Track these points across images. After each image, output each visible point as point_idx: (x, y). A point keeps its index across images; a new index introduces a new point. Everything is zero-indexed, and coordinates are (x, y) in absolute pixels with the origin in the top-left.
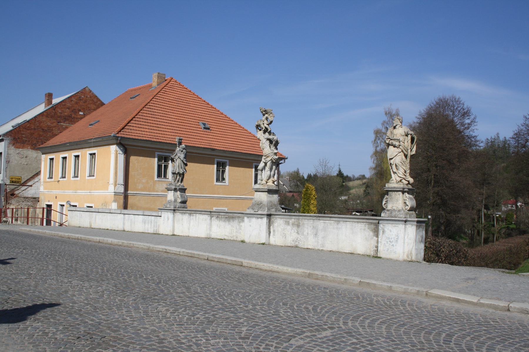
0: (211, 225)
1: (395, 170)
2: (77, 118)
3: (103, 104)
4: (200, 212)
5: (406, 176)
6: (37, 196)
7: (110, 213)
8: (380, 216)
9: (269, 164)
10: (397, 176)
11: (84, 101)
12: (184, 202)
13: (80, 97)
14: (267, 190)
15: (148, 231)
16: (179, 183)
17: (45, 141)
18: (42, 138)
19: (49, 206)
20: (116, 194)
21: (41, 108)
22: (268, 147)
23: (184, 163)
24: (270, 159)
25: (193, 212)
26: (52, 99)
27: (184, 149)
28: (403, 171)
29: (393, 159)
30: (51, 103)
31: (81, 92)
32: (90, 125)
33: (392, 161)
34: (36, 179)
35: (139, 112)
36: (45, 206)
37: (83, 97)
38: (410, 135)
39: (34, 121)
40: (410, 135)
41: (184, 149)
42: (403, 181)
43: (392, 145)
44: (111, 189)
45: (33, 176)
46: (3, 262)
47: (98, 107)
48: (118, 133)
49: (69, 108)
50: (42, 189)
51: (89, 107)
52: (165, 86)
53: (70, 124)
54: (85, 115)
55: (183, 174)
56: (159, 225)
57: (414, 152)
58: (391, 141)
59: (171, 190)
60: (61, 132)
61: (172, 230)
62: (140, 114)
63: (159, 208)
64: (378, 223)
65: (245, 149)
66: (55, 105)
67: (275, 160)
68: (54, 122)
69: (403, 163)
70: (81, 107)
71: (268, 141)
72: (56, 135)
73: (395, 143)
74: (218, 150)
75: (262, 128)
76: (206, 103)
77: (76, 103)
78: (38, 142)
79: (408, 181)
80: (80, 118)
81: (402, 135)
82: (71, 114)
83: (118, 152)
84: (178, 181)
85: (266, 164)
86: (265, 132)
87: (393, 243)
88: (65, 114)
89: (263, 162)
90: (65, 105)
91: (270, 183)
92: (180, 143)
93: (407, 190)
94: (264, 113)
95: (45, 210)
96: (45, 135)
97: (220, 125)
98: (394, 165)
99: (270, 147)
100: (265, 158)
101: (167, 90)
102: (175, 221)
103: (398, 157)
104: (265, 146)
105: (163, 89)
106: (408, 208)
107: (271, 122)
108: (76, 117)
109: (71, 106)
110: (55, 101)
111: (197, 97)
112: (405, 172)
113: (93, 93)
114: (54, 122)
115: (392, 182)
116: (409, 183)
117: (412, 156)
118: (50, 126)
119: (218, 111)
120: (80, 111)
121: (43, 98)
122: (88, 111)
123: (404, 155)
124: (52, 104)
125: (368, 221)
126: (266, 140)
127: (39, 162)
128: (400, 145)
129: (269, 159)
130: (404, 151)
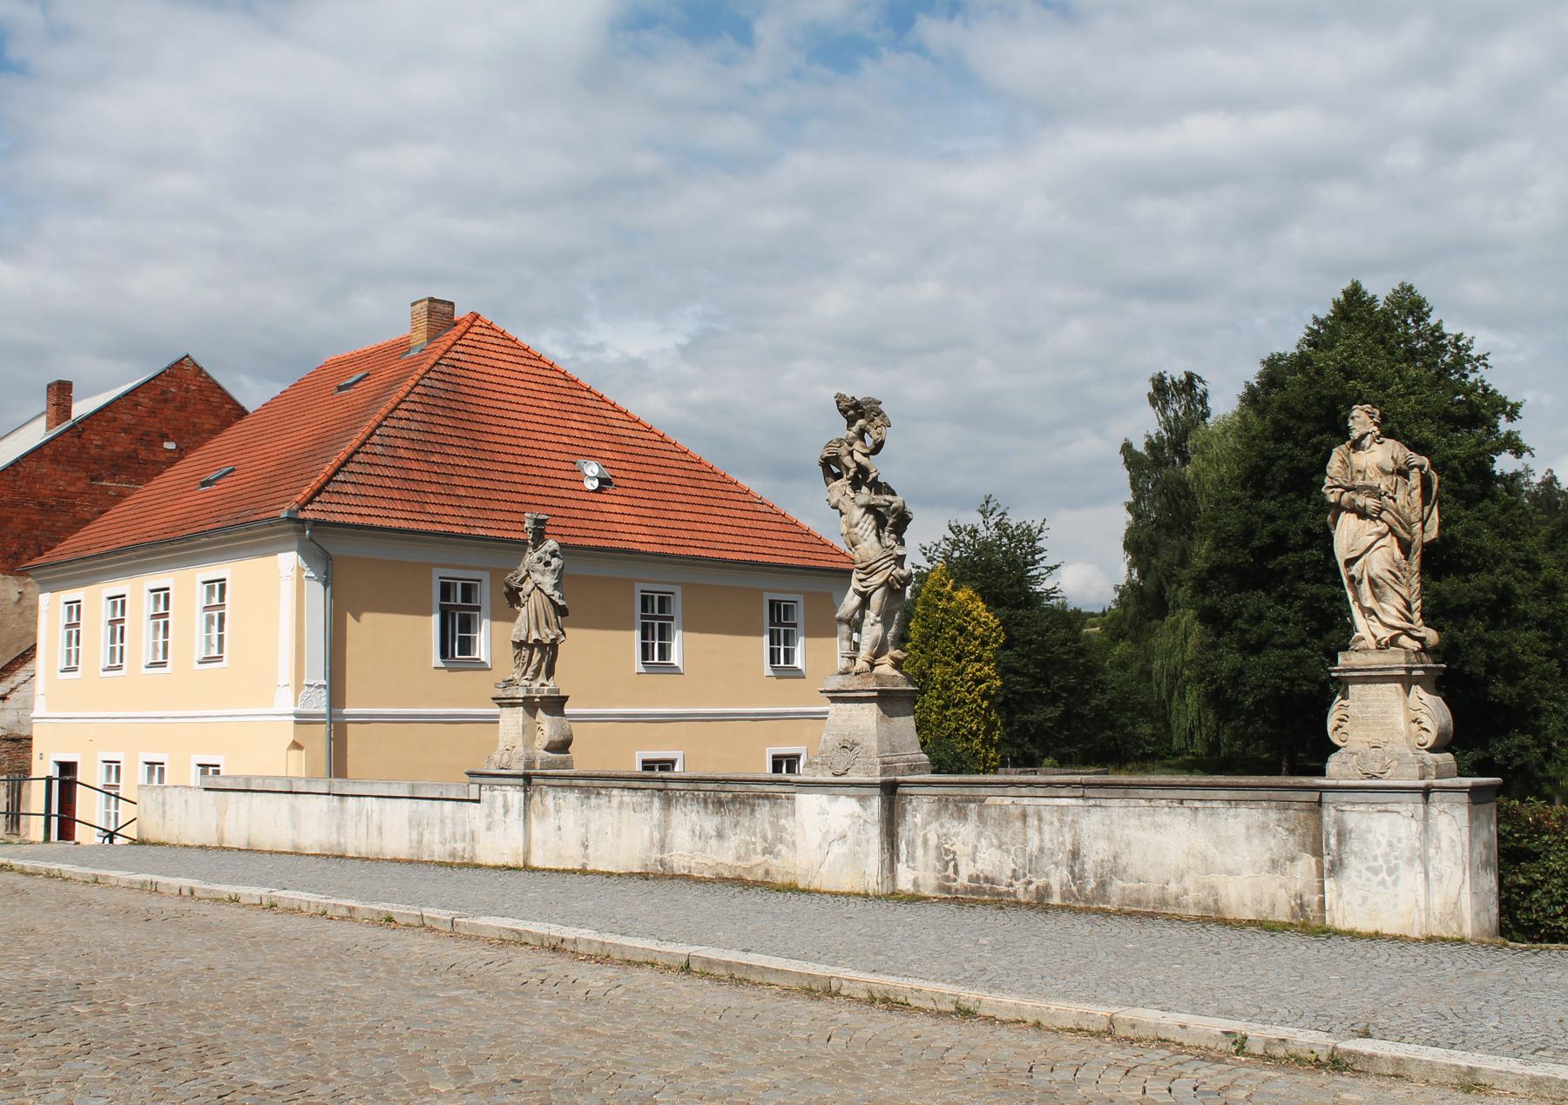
0: (665, 826)
1: (1369, 602)
2: (156, 463)
3: (241, 412)
4: (623, 783)
5: (1410, 621)
6: (24, 733)
7: (291, 792)
8: (1321, 772)
9: (876, 599)
10: (1378, 624)
11: (177, 404)
12: (562, 746)
13: (164, 392)
14: (875, 694)
15: (431, 855)
16: (542, 679)
17: (49, 544)
18: (38, 533)
19: (67, 768)
20: (302, 720)
21: (36, 434)
22: (873, 538)
23: (552, 602)
24: (882, 580)
25: (597, 783)
26: (70, 401)
27: (553, 554)
28: (1399, 603)
29: (1361, 561)
30: (66, 413)
31: (168, 376)
32: (203, 484)
33: (1355, 570)
34: (21, 675)
35: (372, 434)
36: (54, 772)
37: (174, 390)
38: (1416, 470)
39: (11, 478)
40: (1416, 470)
41: (553, 554)
42: (1404, 640)
43: (1352, 510)
44: (286, 703)
45: (10, 663)
46: (3, 698)
47: (227, 424)
48: (303, 510)
49: (126, 431)
50: (40, 709)
51: (194, 424)
52: (455, 344)
53: (131, 483)
54: (181, 453)
55: (554, 645)
56: (473, 833)
57: (1433, 533)
58: (1346, 496)
59: (513, 705)
60: (102, 513)
61: (521, 851)
62: (375, 439)
63: (205, 580)
64: (1320, 803)
65: (736, 548)
66: (81, 422)
67: (898, 582)
68: (79, 479)
69: (1399, 574)
70: (169, 424)
71: (872, 516)
72: (87, 522)
73: (1361, 500)
74: (645, 553)
75: (848, 469)
76: (594, 397)
77: (153, 413)
78: (25, 547)
79: (1421, 640)
80: (164, 463)
81: (1384, 472)
82: (135, 450)
83: (305, 574)
84: (537, 673)
85: (865, 599)
86: (856, 484)
87: (1383, 875)
88: (116, 449)
89: (855, 590)
90: (115, 419)
91: (885, 668)
92: (540, 536)
93: (1421, 673)
94: (851, 412)
95: (56, 784)
96: (50, 523)
97: (645, 468)
98: (1366, 581)
99: (878, 535)
100: (864, 577)
101: (462, 357)
102: (533, 816)
103: (1377, 553)
104: (861, 533)
105: (449, 355)
106: (1430, 739)
107: (878, 447)
108: (152, 458)
109: (134, 422)
110: (81, 408)
111: (562, 376)
112: (1408, 606)
113: (208, 377)
114: (79, 479)
115: (1362, 644)
116: (1424, 649)
117: (1429, 550)
118: (65, 491)
119: (637, 422)
120: (165, 437)
121: (41, 403)
122: (192, 438)
123: (1399, 547)
124: (70, 418)
125: (1274, 794)
126: (863, 510)
127: (28, 614)
128: (1382, 510)
129: (877, 579)
130: (1399, 529)
